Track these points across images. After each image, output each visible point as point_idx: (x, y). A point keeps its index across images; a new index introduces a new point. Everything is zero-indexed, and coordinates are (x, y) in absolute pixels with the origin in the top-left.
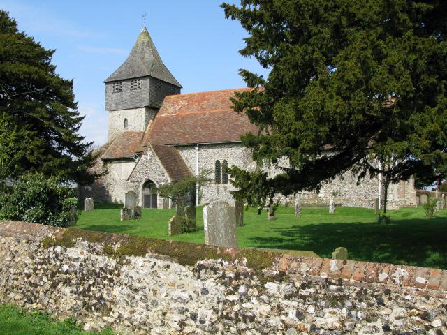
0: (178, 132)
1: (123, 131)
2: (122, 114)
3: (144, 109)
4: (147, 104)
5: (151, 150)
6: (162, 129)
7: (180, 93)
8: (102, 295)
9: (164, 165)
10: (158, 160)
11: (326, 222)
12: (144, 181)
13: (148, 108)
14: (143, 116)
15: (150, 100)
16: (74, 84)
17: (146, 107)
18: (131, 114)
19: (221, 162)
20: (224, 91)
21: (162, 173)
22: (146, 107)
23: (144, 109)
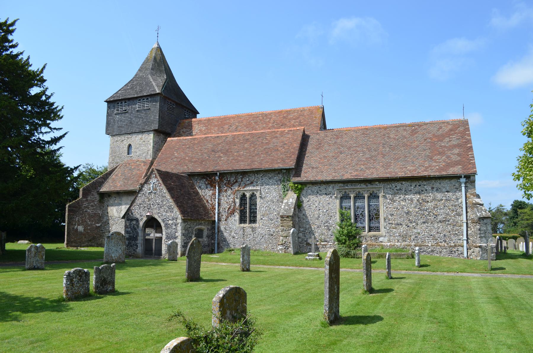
0: (192, 158)
1: (126, 160)
2: (127, 140)
3: (152, 132)
4: (156, 126)
5: (156, 177)
6: (173, 154)
7: (196, 118)
8: (181, 256)
9: (172, 197)
10: (165, 190)
11: (530, 260)
12: (145, 219)
13: (157, 132)
14: (151, 141)
15: (160, 124)
16: (109, 298)
17: (155, 131)
18: (136, 140)
19: (248, 195)
20: (248, 115)
21: (170, 209)
22: (155, 131)
23: (152, 135)
